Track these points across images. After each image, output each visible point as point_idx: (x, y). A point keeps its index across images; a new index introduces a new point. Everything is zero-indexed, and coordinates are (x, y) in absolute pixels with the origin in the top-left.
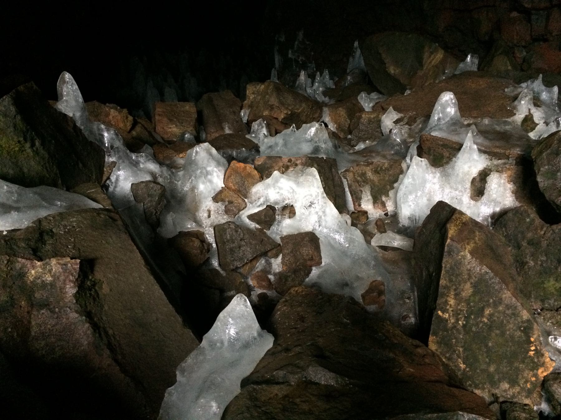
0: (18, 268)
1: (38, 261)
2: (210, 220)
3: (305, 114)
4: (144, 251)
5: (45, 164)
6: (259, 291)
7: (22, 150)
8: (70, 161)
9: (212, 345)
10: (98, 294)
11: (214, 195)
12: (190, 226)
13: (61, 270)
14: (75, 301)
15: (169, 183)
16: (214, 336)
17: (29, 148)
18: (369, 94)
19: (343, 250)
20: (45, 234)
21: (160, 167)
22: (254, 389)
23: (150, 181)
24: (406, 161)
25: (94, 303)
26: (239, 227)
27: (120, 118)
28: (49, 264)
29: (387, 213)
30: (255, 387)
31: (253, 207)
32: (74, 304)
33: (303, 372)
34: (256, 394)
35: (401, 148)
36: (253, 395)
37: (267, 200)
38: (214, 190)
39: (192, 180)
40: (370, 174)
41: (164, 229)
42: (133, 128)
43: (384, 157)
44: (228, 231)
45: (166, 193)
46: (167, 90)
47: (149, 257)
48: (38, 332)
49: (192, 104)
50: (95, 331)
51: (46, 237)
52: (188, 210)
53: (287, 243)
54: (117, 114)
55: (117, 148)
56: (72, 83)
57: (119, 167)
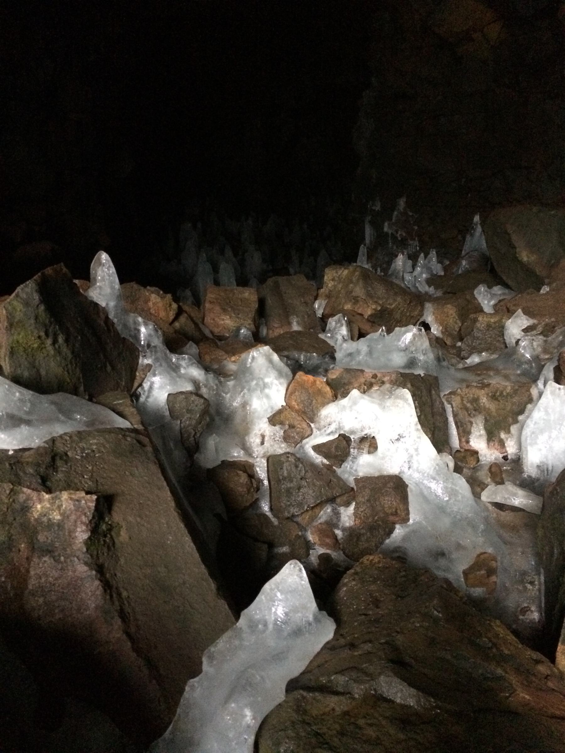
0: (21, 500)
1: (47, 493)
2: (263, 448)
3: (399, 311)
4: (176, 485)
5: (67, 365)
7: (41, 347)
8: (95, 361)
9: (253, 625)
10: (114, 543)
11: (271, 414)
12: (237, 454)
14: (85, 550)
16: (256, 613)
17: (51, 345)
18: (490, 287)
20: (58, 458)
21: (206, 374)
22: (304, 698)
23: (191, 393)
24: (537, 386)
26: (301, 460)
28: (59, 499)
29: (507, 456)
31: (321, 435)
33: (372, 682)
34: (306, 705)
35: (531, 367)
37: (340, 428)
38: (272, 408)
39: (244, 394)
40: (484, 401)
41: (203, 456)
42: (176, 318)
43: (506, 377)
44: (286, 465)
45: (210, 409)
47: (181, 495)
48: (37, 585)
50: (105, 591)
51: (59, 463)
52: (236, 433)
54: (159, 300)
55: (155, 347)
56: (109, 266)
57: (155, 371)
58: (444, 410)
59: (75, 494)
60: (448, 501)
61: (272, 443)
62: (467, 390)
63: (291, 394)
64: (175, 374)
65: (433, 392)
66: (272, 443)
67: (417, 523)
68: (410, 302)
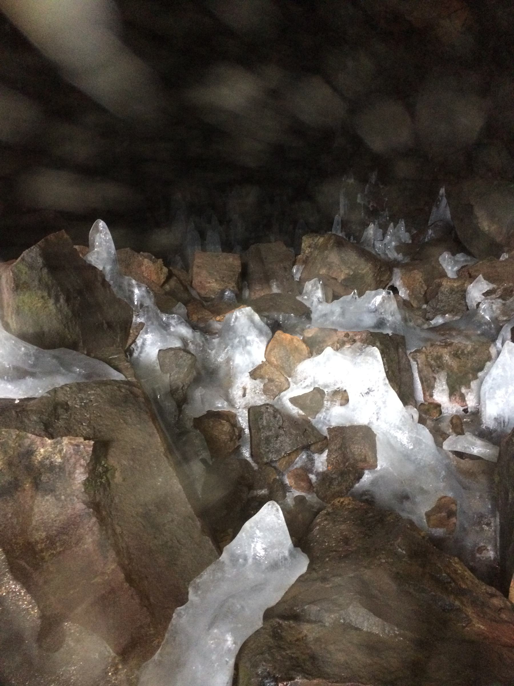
0: (26, 445)
1: (49, 439)
6: (297, 493)
9: (234, 559)
10: (109, 484)
11: (252, 369)
12: (221, 405)
13: (72, 451)
14: (83, 490)
15: (202, 351)
17: (53, 304)
18: (454, 254)
19: (405, 453)
20: (59, 407)
21: (193, 332)
22: (280, 625)
23: (179, 349)
24: (495, 345)
25: (104, 494)
26: (277, 412)
27: (153, 269)
29: (467, 409)
30: (281, 622)
31: (298, 388)
32: (82, 493)
35: (490, 328)
36: (278, 633)
37: (315, 382)
38: (253, 364)
40: (447, 358)
43: (468, 337)
46: (209, 233)
49: (237, 256)
51: (60, 411)
53: (336, 436)
54: (151, 264)
55: (147, 307)
56: (106, 233)
57: (147, 329)
58: (410, 366)
59: (75, 440)
60: (412, 449)
61: (253, 395)
62: (431, 349)
63: (271, 350)
64: (165, 332)
65: (400, 350)
66: (253, 395)
67: (384, 469)
68: (381, 267)
